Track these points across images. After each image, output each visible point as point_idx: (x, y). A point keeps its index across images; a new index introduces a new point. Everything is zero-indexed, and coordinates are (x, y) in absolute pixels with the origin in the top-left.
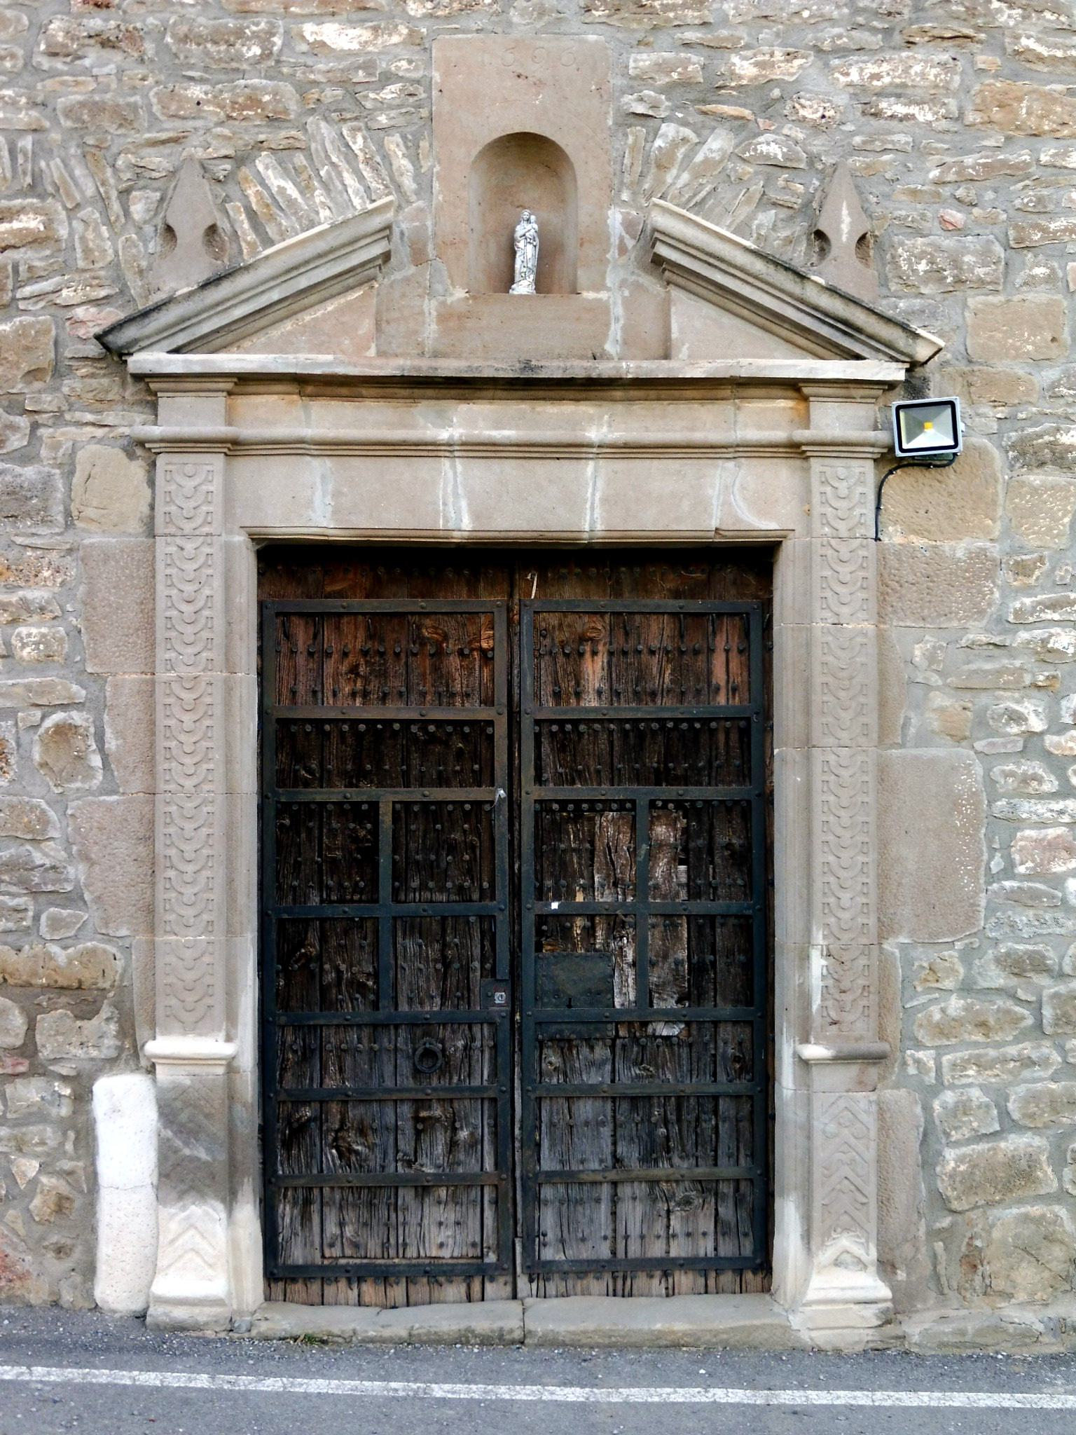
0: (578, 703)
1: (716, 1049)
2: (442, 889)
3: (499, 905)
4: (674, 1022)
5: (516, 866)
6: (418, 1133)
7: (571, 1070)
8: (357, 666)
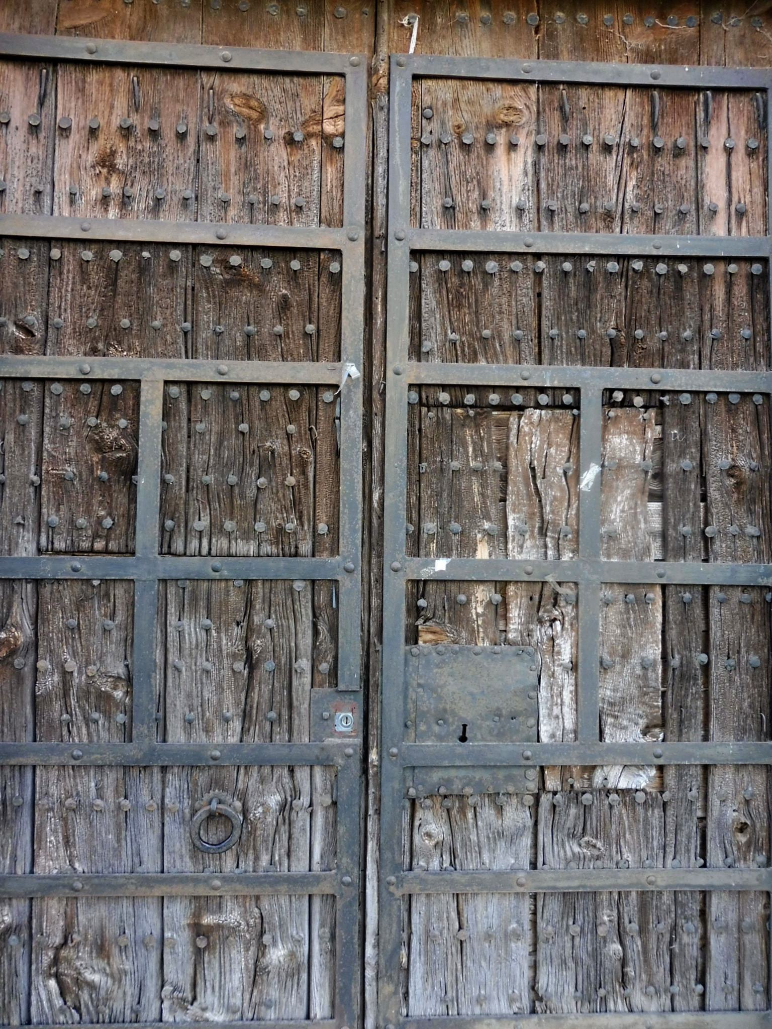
0: (484, 225)
1: (705, 808)
2: (248, 534)
3: (346, 561)
4: (640, 767)
5: (376, 496)
6: (199, 953)
7: (464, 845)
8: (113, 153)
